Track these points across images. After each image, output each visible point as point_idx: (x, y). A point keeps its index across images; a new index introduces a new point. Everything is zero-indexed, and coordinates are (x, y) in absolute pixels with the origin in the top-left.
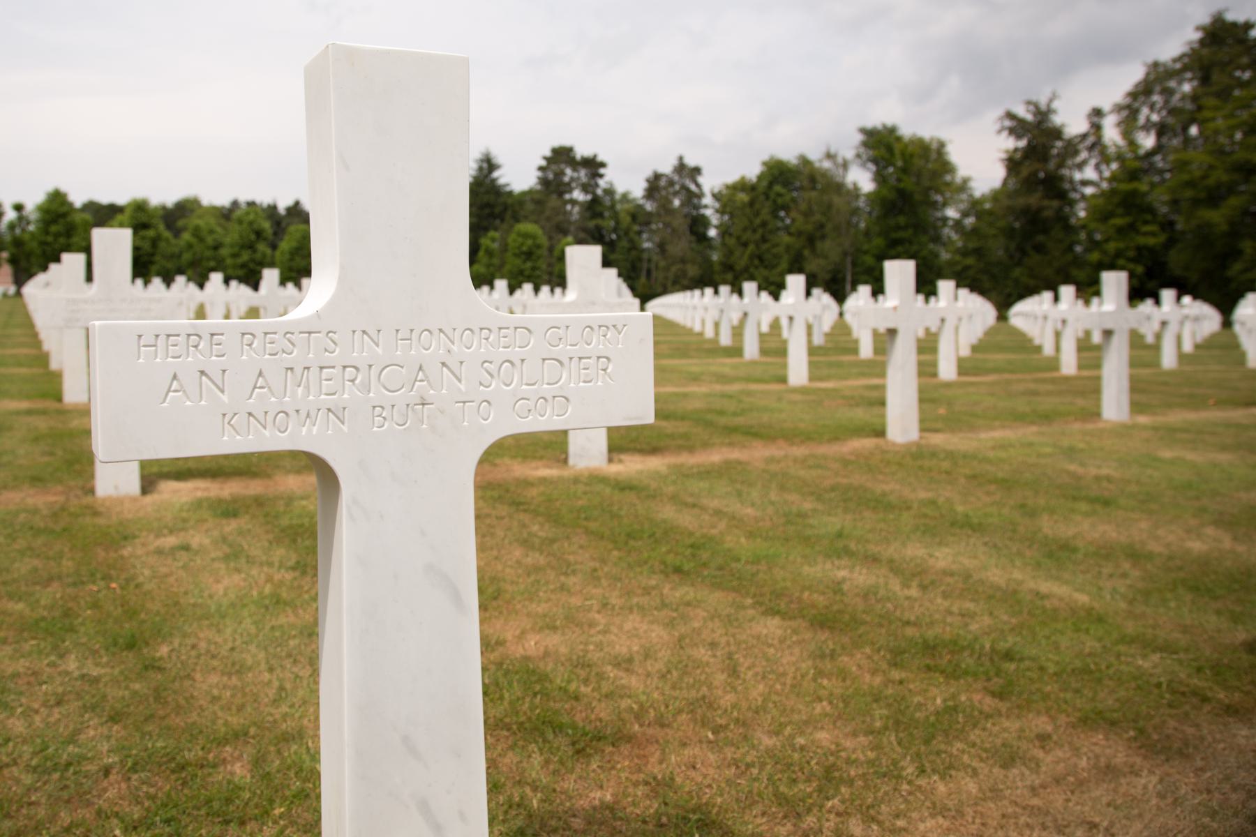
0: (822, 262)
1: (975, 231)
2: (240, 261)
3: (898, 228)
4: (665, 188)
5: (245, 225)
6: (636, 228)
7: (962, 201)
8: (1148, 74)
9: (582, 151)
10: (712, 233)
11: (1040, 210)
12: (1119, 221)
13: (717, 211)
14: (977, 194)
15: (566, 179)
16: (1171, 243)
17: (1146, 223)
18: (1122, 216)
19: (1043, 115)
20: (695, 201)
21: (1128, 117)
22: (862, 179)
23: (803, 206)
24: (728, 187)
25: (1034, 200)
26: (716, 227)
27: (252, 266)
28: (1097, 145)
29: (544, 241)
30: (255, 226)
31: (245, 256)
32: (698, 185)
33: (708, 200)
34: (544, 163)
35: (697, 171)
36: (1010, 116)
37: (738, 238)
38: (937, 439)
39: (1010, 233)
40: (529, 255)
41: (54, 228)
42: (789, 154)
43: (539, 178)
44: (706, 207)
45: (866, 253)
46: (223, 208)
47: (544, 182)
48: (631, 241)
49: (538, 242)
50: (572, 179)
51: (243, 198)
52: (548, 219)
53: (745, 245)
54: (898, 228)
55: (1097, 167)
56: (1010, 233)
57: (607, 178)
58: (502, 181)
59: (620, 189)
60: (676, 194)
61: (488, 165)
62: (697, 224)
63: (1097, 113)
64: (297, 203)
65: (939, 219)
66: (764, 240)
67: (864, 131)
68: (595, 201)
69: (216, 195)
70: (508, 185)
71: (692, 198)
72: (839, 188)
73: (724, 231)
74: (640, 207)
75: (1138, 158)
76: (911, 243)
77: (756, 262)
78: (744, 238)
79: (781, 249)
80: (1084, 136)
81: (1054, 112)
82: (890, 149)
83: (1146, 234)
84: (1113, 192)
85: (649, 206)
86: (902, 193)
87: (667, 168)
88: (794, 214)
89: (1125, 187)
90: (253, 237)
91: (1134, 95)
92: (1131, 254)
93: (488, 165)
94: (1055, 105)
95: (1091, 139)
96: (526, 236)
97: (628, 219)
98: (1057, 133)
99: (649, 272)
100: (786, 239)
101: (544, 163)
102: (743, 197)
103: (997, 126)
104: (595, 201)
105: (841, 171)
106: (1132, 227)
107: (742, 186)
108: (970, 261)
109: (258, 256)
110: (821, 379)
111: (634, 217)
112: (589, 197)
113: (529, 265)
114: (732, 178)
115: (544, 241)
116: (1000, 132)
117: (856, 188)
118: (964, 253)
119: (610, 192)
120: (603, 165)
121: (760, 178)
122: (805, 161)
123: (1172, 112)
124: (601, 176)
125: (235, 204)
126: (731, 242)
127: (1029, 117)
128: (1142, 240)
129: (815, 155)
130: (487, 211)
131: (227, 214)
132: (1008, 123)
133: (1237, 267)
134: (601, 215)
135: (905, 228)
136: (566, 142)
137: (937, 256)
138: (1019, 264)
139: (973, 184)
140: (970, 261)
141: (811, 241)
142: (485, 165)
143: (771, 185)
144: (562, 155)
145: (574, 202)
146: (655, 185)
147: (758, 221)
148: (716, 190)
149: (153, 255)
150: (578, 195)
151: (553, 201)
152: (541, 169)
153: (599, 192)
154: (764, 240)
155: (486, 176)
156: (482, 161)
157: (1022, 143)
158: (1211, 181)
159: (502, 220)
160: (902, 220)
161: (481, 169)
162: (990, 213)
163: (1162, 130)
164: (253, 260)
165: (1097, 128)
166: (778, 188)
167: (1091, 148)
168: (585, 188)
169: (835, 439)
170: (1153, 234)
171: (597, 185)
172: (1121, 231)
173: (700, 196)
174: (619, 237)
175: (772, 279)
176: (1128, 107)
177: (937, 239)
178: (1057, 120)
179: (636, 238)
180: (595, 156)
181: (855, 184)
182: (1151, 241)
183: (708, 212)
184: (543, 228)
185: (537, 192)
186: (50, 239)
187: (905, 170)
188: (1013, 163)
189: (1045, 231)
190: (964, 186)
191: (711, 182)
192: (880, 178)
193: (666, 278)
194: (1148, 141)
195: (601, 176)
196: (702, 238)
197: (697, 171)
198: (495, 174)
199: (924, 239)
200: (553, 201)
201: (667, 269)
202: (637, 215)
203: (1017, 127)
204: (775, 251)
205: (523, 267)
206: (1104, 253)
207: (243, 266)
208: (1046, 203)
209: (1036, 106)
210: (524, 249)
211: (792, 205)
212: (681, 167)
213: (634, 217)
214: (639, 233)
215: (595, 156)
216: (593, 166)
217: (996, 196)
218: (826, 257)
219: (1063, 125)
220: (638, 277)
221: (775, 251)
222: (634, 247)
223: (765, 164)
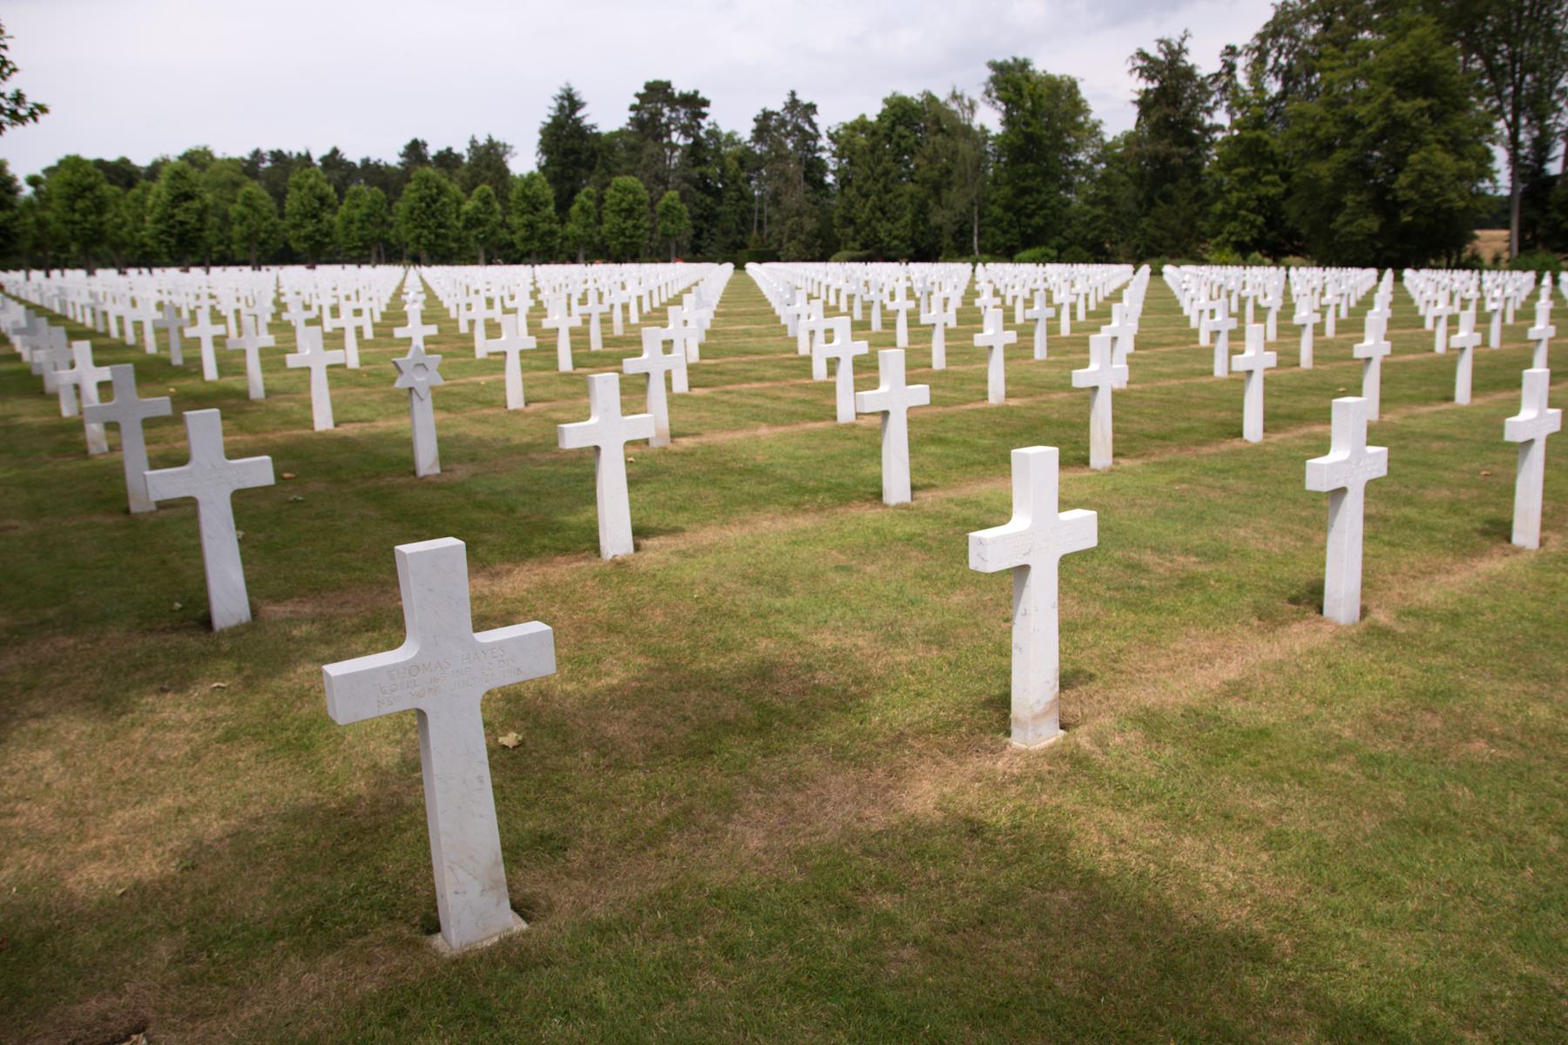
0: (948, 213)
1: (1105, 179)
2: (303, 232)
3: (1027, 176)
4: (776, 129)
5: (305, 190)
6: (744, 175)
7: (1095, 146)
8: (1276, 17)
9: (681, 87)
10: (830, 179)
11: (1168, 157)
12: (1241, 171)
13: (834, 154)
14: (1108, 139)
15: (664, 120)
16: (1288, 193)
17: (1268, 172)
18: (1245, 165)
19: (1174, 53)
20: (811, 143)
21: (1256, 60)
22: (990, 119)
23: (928, 151)
24: (846, 127)
25: (1162, 147)
26: (833, 172)
27: (318, 237)
28: (1230, 88)
29: (645, 195)
30: (318, 191)
31: (310, 227)
32: (813, 125)
33: (824, 142)
34: (637, 101)
35: (812, 108)
36: (1142, 55)
37: (859, 188)
38: (953, 368)
39: (1139, 180)
40: (630, 212)
41: (80, 204)
42: (912, 91)
43: (631, 119)
44: (822, 149)
45: (994, 203)
46: (243, 160)
47: (637, 122)
48: (739, 190)
49: (640, 196)
50: (671, 121)
51: (267, 147)
52: (645, 168)
53: (866, 196)
54: (1027, 176)
55: (1229, 109)
56: (1139, 180)
57: (709, 119)
58: (587, 122)
59: (725, 129)
60: (788, 135)
61: (570, 103)
62: (814, 169)
63: (1231, 51)
64: (335, 151)
65: (1070, 163)
66: (887, 190)
67: (993, 66)
68: (698, 143)
69: (231, 145)
70: (593, 126)
71: (807, 139)
72: (967, 131)
73: (844, 180)
74: (748, 149)
75: (1263, 104)
76: (1039, 192)
77: (879, 214)
78: (864, 190)
79: (904, 200)
80: (1217, 76)
81: (1186, 51)
82: (1018, 91)
83: (1266, 184)
84: (1238, 140)
85: (758, 149)
86: (1030, 138)
87: (777, 105)
88: (917, 160)
89: (1248, 135)
90: (317, 204)
91: (1262, 37)
92: (1253, 204)
93: (570, 103)
94: (1185, 45)
95: (1225, 79)
96: (626, 190)
97: (736, 164)
98: (1189, 73)
99: (760, 223)
100: (911, 187)
101: (637, 101)
102: (861, 139)
103: (1129, 67)
104: (698, 143)
105: (967, 113)
106: (1254, 176)
107: (860, 125)
108: (1099, 211)
109: (324, 226)
110: (916, 344)
111: (741, 162)
112: (690, 141)
113: (630, 223)
114: (850, 117)
115: (645, 195)
116: (1131, 72)
117: (984, 130)
118: (1093, 202)
119: (714, 134)
120: (706, 103)
121: (880, 117)
122: (931, 99)
123: (1302, 55)
124: (704, 116)
125: (257, 154)
126: (851, 192)
127: (1161, 57)
128: (1263, 190)
129: (942, 95)
130: (572, 158)
131: (250, 167)
132: (1139, 63)
133: (1341, 219)
134: (705, 162)
135: (1035, 174)
136: (663, 77)
137: (1203, 121)
138: (1146, 215)
139: (1103, 128)
140: (1099, 211)
141: (936, 189)
142: (566, 103)
143: (893, 125)
144: (657, 92)
145: (674, 147)
146: (764, 124)
147: (879, 169)
148: (832, 131)
149: (200, 230)
150: (677, 138)
151: (651, 147)
152: (633, 108)
153: (702, 134)
154: (887, 190)
155: (569, 116)
156: (562, 98)
157: (1155, 85)
158: (1320, 134)
159: (591, 168)
160: (1030, 167)
161: (561, 108)
162: (1120, 159)
163: (1288, 76)
164: (318, 230)
165: (1230, 68)
166: (901, 129)
167: (1224, 89)
168: (685, 131)
169: (960, 404)
170: (1274, 184)
171: (700, 127)
172: (1243, 180)
173: (816, 137)
174: (725, 185)
175: (895, 233)
176: (1258, 49)
177: (1068, 186)
178: (1189, 60)
179: (744, 186)
180: (696, 92)
181: (982, 127)
182: (1272, 191)
183: (825, 156)
184: (641, 179)
185: (629, 133)
186: (77, 217)
187: (1033, 113)
188: (1146, 104)
189: (1174, 180)
190: (1094, 130)
191: (830, 118)
192: (1009, 121)
193: (781, 233)
194: (1274, 87)
195: (704, 116)
196: (820, 185)
197: (812, 108)
198: (579, 114)
199: (1053, 187)
200: (651, 147)
201: (782, 222)
202: (745, 158)
203: (1149, 67)
204: (897, 202)
205: (624, 226)
206: (1227, 203)
207: (307, 238)
208: (1175, 149)
209: (1168, 45)
210: (624, 205)
211: (916, 148)
212: (793, 104)
213: (741, 162)
214: (749, 179)
215: (696, 92)
216: (694, 104)
217: (1130, 139)
218: (952, 208)
219: (1193, 67)
220: (750, 231)
221: (897, 202)
222: (743, 196)
223: (886, 101)
